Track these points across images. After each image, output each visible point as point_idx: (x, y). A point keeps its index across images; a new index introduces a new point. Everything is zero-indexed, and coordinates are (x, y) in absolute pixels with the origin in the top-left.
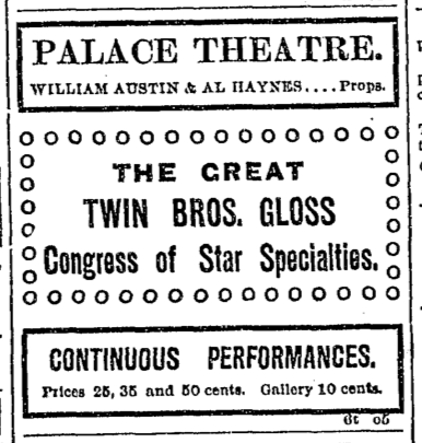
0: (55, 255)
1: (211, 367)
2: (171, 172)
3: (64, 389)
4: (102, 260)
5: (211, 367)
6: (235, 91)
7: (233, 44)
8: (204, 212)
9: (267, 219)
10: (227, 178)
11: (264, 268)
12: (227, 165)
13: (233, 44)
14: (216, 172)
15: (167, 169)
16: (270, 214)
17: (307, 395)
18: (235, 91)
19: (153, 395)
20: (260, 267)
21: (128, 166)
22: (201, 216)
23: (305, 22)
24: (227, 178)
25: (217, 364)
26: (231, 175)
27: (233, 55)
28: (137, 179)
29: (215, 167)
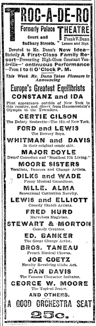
0: (37, 87)
1: (21, 31)
2: (40, 283)
3: (12, 54)
4: (19, 88)
5: (21, 31)
6: (60, 123)
7: (61, 121)
8: (82, 15)
9: (36, 90)
10: (71, 166)
11: (78, 307)
12: (71, 163)
13: (61, 121)
14: (54, 116)
15: (40, 259)
16: (37, 88)
17: (37, 45)
18: (60, 123)
19: (58, 98)
20: (83, 300)
21: (38, 115)
22: (80, 17)
23: (2, 8)
24: (71, 166)
25: (23, 30)
26: (72, 165)
27: (61, 122)
28: (53, 296)
29: (54, 115)
